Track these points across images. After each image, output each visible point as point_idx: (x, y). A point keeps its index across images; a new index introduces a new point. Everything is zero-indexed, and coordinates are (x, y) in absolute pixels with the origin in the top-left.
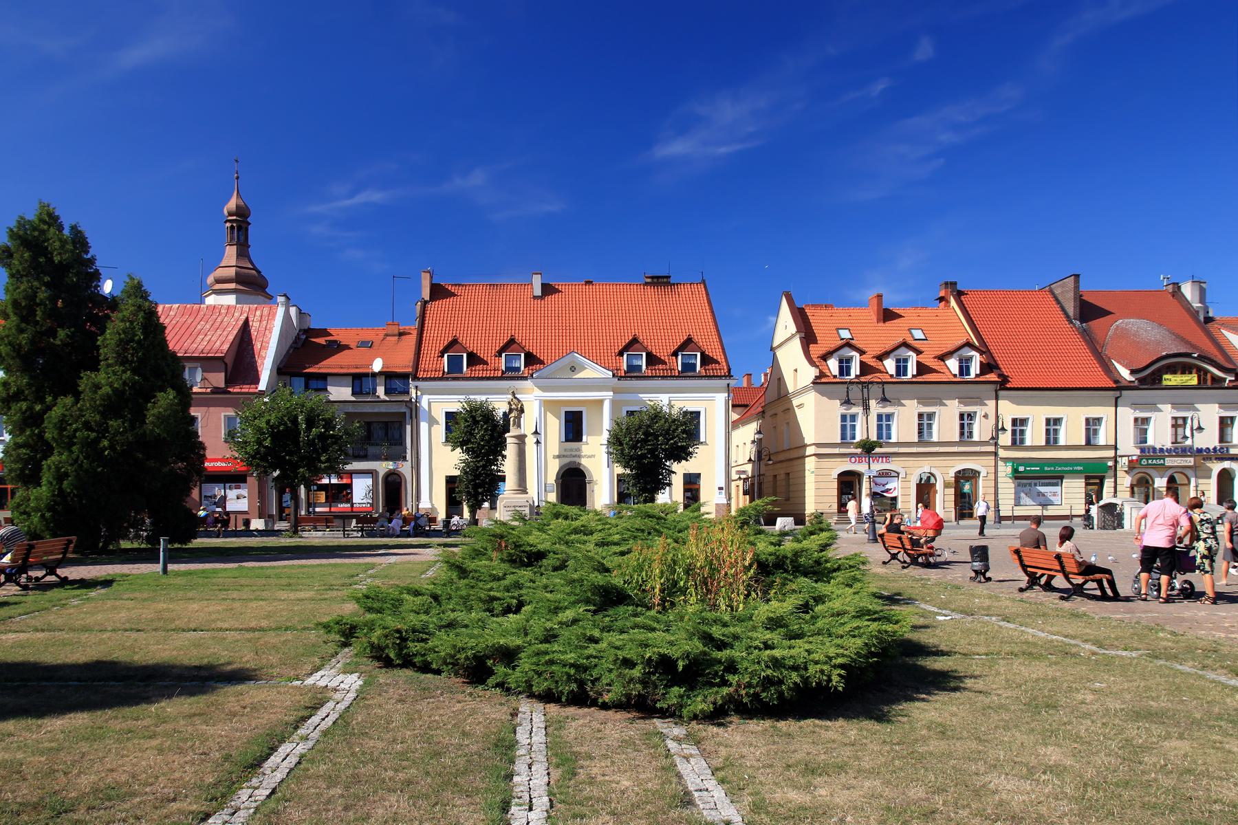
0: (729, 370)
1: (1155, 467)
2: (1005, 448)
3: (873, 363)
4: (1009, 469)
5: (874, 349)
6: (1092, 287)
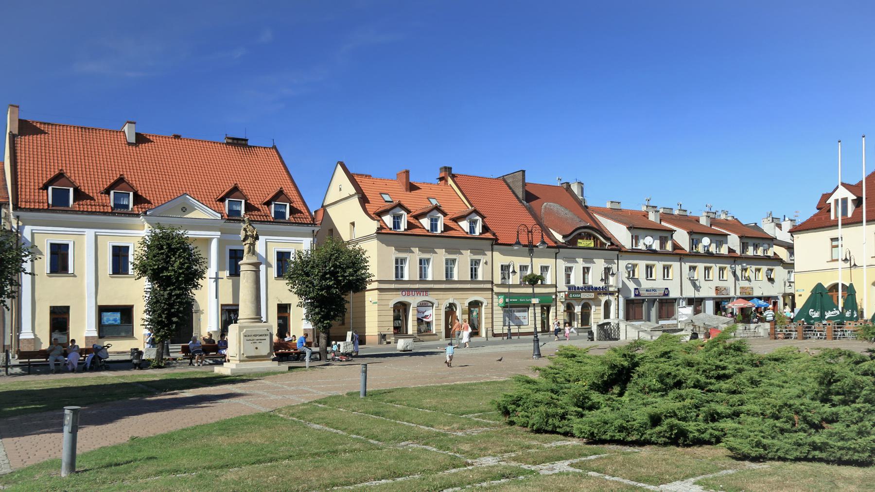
2: (498, 286)
3: (451, 224)
4: (501, 301)
5: (454, 211)
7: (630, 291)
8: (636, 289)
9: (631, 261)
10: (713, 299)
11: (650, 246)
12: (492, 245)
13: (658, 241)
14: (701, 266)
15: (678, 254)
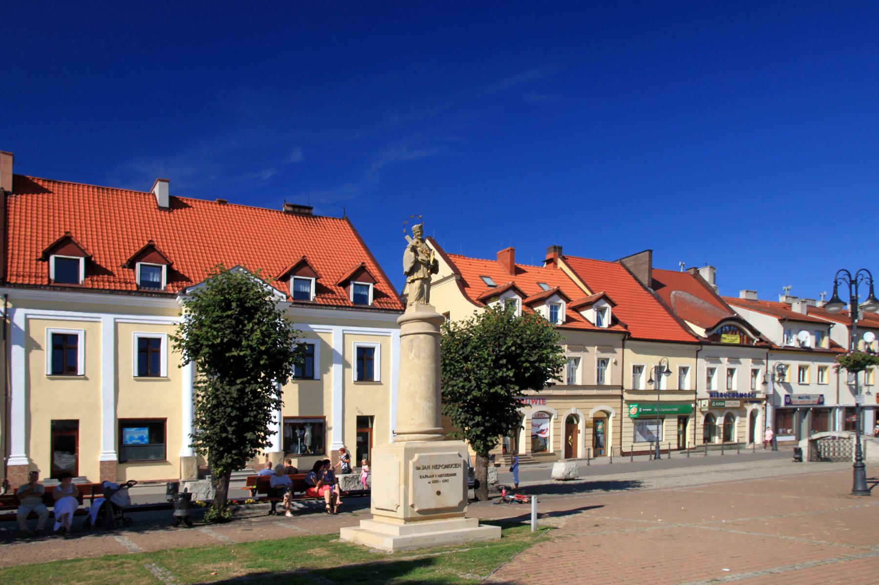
3: (573, 315)
7: (779, 398)
8: (787, 396)
9: (782, 362)
10: (873, 408)
11: (803, 343)
12: (624, 340)
13: (814, 337)
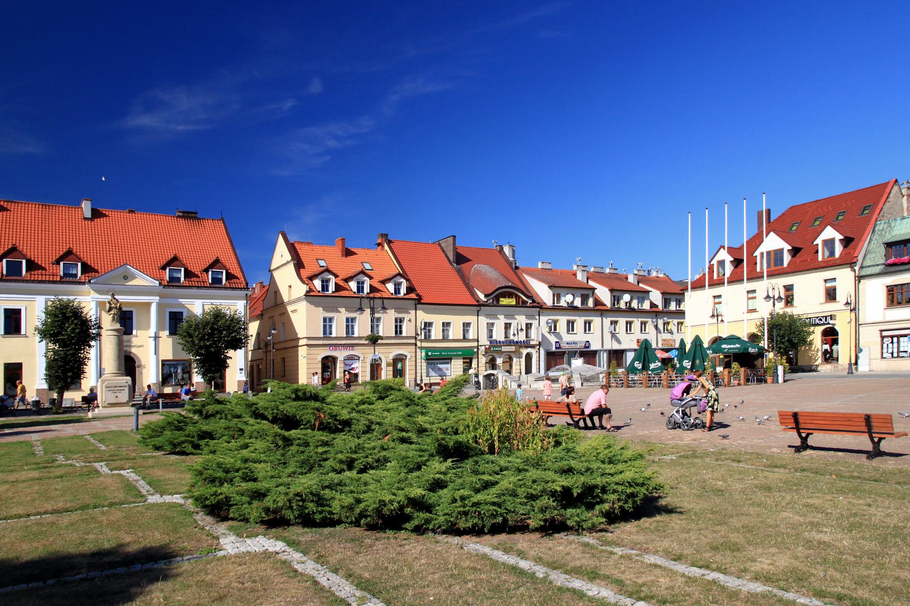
0: (247, 284)
1: (497, 352)
3: (342, 283)
4: (423, 354)
5: (378, 276)
6: (465, 243)
14: (622, 321)
15: (599, 309)
